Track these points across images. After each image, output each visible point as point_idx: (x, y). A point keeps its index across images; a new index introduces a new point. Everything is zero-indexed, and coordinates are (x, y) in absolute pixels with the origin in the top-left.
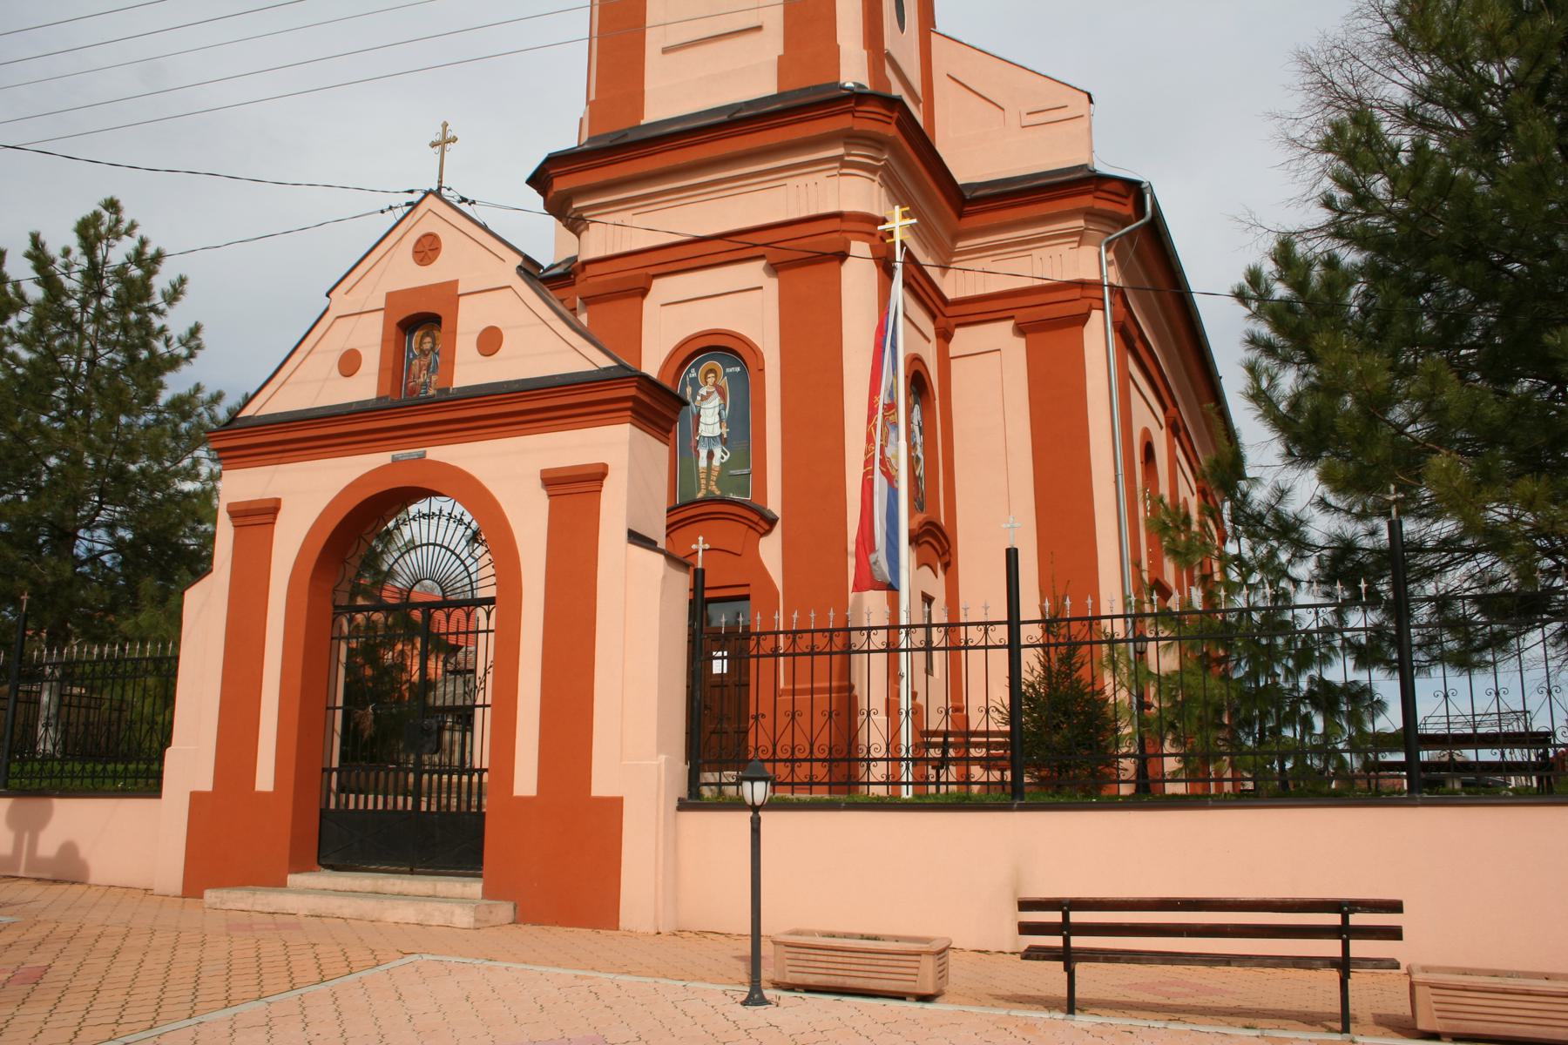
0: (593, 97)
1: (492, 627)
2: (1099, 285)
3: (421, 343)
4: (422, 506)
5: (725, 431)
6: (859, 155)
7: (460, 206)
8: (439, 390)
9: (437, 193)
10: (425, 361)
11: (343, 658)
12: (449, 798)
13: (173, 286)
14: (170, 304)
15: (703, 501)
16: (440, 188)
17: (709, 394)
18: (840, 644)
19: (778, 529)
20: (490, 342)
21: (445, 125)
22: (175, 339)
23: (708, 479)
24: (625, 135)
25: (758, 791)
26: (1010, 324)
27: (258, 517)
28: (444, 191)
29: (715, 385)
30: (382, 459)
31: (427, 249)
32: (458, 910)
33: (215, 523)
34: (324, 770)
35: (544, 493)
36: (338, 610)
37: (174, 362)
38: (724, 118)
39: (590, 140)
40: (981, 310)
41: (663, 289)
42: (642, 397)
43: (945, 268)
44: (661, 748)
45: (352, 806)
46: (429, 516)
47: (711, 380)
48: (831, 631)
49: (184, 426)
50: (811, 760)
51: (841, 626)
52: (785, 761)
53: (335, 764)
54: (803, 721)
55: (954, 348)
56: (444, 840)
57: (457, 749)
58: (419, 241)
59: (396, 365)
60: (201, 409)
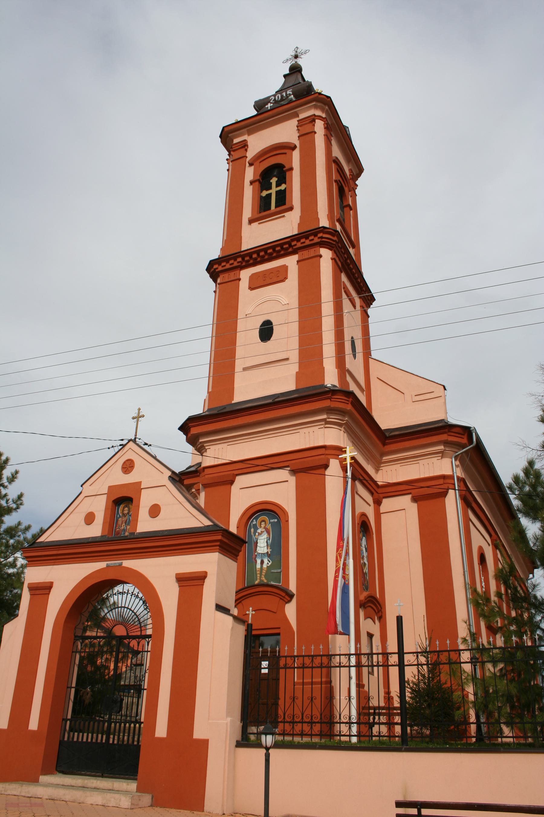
0: (210, 390)
1: (149, 649)
2: (452, 477)
3: (123, 510)
4: (119, 588)
5: (269, 550)
6: (333, 418)
7: (144, 447)
8: (130, 533)
9: (134, 441)
10: (124, 519)
11: (77, 662)
12: (124, 736)
13: (12, 475)
14: (10, 483)
15: (259, 585)
16: (135, 438)
17: (262, 532)
18: (325, 663)
19: (294, 600)
20: (155, 511)
21: (139, 409)
22: (11, 500)
23: (261, 574)
24: (225, 408)
25: (268, 740)
26: (409, 497)
27: (42, 590)
28: (137, 440)
29: (265, 528)
30: (102, 565)
31: (128, 467)
32: (123, 798)
33: (22, 590)
34: (63, 720)
35: (177, 585)
36: (76, 638)
37: (9, 511)
38: (271, 401)
39: (209, 410)
41: (241, 481)
42: (225, 540)
43: (377, 470)
44: (228, 714)
45: (75, 739)
46: (122, 593)
47: (263, 525)
48: (313, 656)
49: (12, 541)
50: (302, 722)
53: (69, 717)
54: (299, 702)
55: (382, 509)
56: (118, 760)
57: (135, 707)
58: (125, 462)
59: (111, 520)
60: (20, 533)
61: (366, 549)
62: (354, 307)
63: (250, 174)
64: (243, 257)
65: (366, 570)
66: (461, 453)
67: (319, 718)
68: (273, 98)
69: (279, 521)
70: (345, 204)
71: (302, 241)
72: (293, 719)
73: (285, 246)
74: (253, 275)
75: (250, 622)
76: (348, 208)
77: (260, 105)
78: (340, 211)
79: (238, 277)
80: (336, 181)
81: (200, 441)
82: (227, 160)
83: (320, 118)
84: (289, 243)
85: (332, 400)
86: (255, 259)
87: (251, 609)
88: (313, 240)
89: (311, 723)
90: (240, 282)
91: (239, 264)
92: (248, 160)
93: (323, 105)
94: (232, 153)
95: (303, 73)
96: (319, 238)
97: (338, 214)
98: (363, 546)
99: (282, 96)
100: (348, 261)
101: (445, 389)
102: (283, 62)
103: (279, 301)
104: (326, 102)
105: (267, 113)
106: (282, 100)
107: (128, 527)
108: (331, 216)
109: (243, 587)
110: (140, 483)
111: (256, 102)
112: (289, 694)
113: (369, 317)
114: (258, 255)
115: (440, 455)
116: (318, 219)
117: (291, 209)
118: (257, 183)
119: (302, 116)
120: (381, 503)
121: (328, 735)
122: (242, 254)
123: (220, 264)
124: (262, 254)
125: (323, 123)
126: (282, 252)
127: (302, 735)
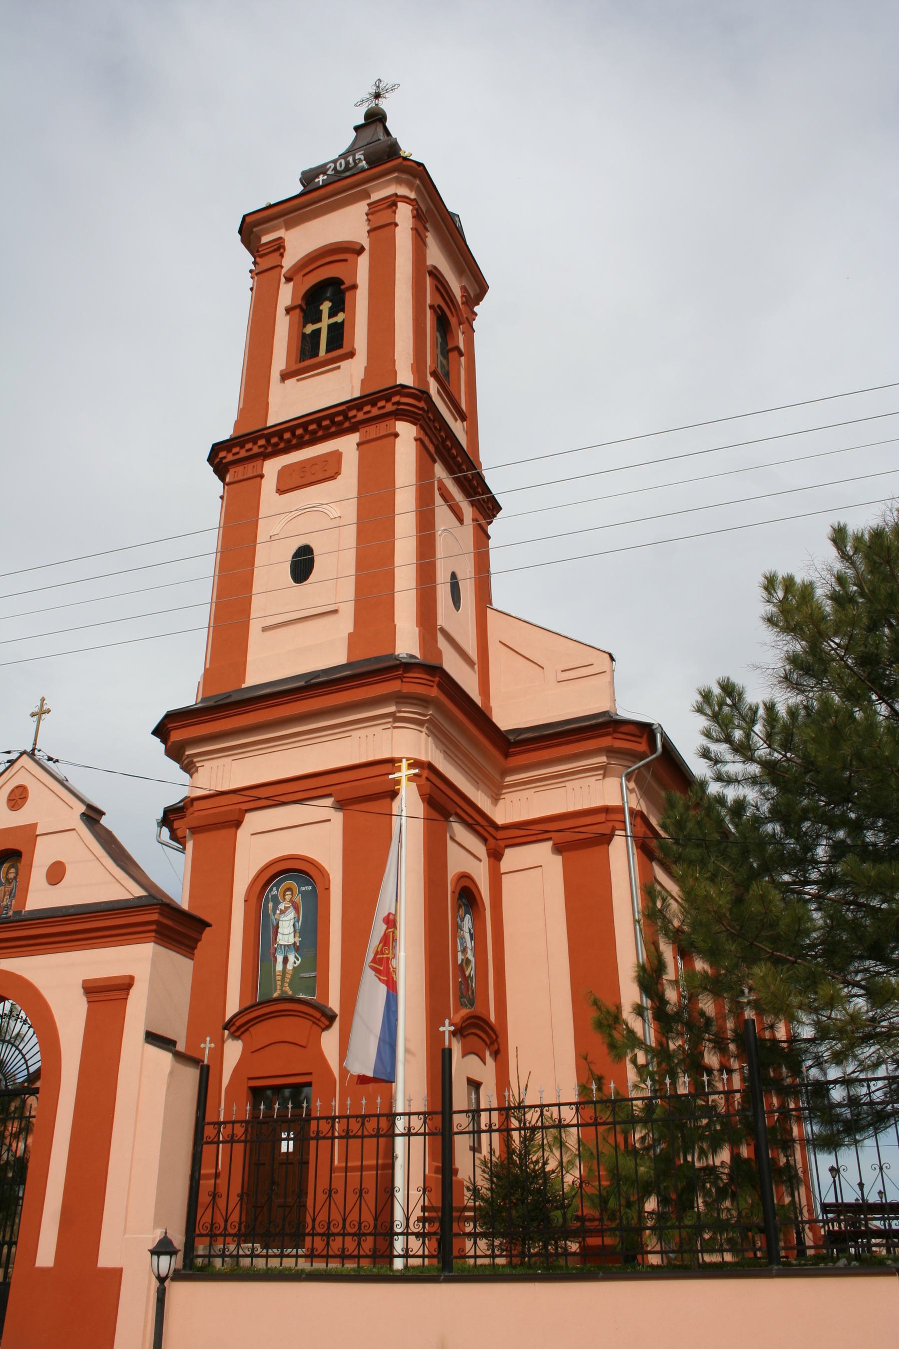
0: (208, 666)
2: (620, 810)
3: (7, 873)
5: (298, 940)
6: (408, 711)
9: (32, 754)
10: (9, 888)
17: (286, 908)
20: (56, 873)
21: (43, 700)
23: (283, 981)
24: (230, 696)
26: (549, 844)
29: (291, 901)
31: (18, 798)
35: (84, 1000)
38: (302, 683)
39: (203, 700)
40: (528, 832)
41: (254, 821)
42: (165, 921)
43: (496, 799)
47: (288, 897)
48: (364, 1117)
50: (344, 1235)
51: (386, 1111)
52: (353, 1235)
54: (338, 1198)
58: (13, 791)
61: (471, 935)
62: (461, 521)
63: (286, 295)
64: (268, 438)
65: (470, 971)
66: (639, 768)
67: (236, 1229)
68: (332, 165)
69: (314, 888)
70: (450, 346)
71: (366, 409)
72: (329, 1228)
73: (337, 419)
74: (284, 467)
75: (206, 1062)
76: (456, 353)
77: (308, 178)
78: (440, 357)
79: (259, 473)
80: (431, 307)
81: (187, 753)
82: (251, 271)
83: (405, 199)
84: (344, 413)
85: (404, 680)
86: (289, 441)
87: (208, 1039)
88: (384, 407)
89: (359, 1235)
90: (264, 481)
91: (262, 450)
92: (284, 271)
93: (410, 177)
94: (258, 260)
95: (387, 124)
96: (394, 404)
97: (433, 361)
98: (466, 929)
99: (347, 163)
100: (448, 443)
101: (612, 659)
102: (356, 105)
103: (318, 513)
104: (417, 173)
105: (321, 190)
106: (347, 168)
107: (13, 902)
108: (418, 366)
109: (253, 1002)
110: (34, 826)
111: (304, 173)
112: (323, 1184)
113: (489, 537)
114: (293, 434)
115: (601, 772)
116: (395, 373)
117: (351, 354)
118: (297, 311)
119: (376, 196)
120: (503, 855)
121: (323, 1256)
122: (266, 432)
123: (229, 451)
124: (299, 432)
125: (411, 207)
126: (333, 429)
127: (343, 1257)
